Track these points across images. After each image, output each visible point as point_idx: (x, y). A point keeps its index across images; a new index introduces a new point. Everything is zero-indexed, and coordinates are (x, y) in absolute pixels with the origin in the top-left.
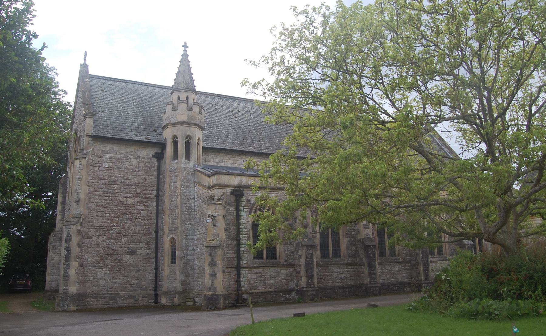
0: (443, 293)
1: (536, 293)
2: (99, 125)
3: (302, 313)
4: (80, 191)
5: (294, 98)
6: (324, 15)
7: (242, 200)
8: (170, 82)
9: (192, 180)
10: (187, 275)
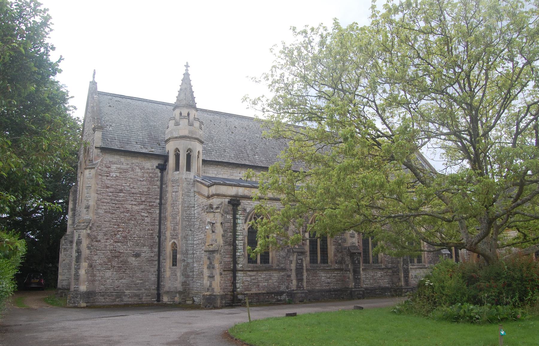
0: (426, 297)
1: (513, 300)
2: (107, 137)
3: (294, 314)
4: (90, 198)
5: (291, 113)
6: (321, 36)
7: (239, 209)
8: (173, 100)
9: (192, 190)
10: (187, 276)
